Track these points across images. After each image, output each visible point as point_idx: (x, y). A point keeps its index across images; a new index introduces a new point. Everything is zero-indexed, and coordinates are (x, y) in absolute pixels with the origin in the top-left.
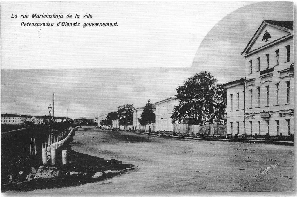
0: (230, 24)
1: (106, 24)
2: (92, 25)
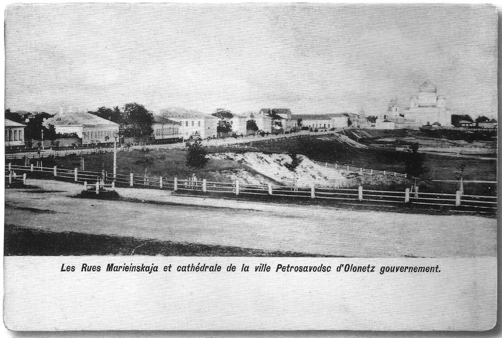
0: (472, 97)
1: (420, 268)
2: (395, 269)
